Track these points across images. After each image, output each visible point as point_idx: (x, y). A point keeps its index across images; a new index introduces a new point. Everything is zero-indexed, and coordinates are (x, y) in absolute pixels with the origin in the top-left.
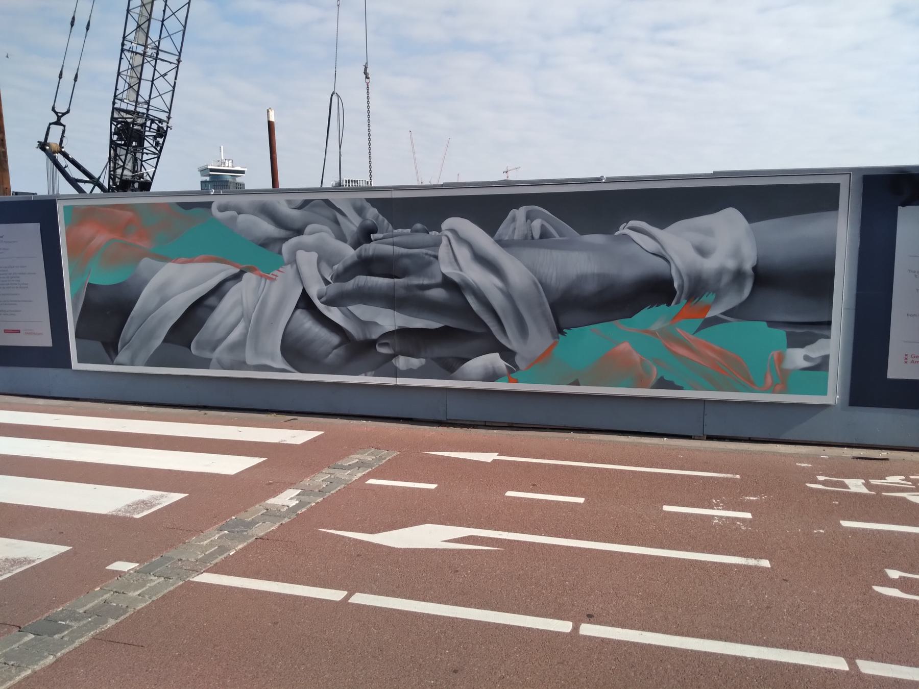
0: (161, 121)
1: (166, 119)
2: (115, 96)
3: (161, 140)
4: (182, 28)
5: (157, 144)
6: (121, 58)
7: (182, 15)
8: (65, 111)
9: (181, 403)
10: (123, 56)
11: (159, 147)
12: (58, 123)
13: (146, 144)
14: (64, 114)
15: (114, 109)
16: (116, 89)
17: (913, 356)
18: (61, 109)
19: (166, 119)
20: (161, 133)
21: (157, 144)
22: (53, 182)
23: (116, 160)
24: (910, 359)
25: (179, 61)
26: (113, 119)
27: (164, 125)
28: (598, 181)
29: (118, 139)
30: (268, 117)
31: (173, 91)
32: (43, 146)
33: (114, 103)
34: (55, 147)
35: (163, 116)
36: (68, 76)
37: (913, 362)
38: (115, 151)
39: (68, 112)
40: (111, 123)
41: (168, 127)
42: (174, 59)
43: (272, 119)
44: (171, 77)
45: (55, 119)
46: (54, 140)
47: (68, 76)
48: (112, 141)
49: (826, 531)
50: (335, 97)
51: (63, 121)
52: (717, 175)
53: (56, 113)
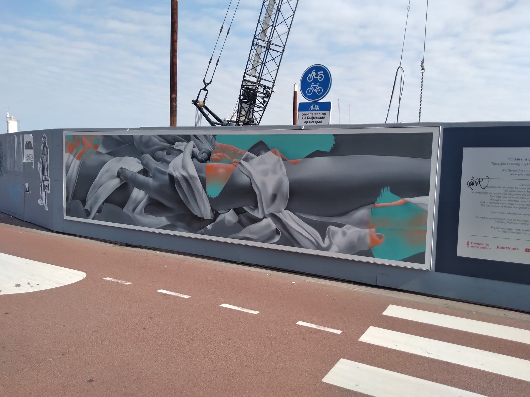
0: (269, 88)
1: (271, 87)
2: (245, 73)
3: (267, 100)
4: (288, 30)
5: (264, 101)
6: (251, 49)
7: (289, 21)
8: (209, 82)
9: (340, 277)
10: (253, 48)
11: (265, 104)
12: (205, 89)
13: (257, 102)
14: (208, 84)
15: (244, 80)
16: (246, 68)
17: (472, 243)
18: (207, 81)
19: (271, 87)
20: (268, 95)
21: (264, 101)
22: (198, 120)
23: (241, 111)
24: (470, 245)
25: (283, 51)
26: (242, 86)
27: (270, 91)
28: (124, 130)
29: (243, 99)
30: (294, 89)
31: (278, 69)
32: (195, 103)
33: (244, 77)
34: (202, 104)
35: (270, 85)
36: (214, 61)
37: (472, 246)
38: (241, 105)
39: (210, 83)
40: (241, 89)
41: (272, 91)
42: (280, 49)
43: (296, 90)
44: (277, 60)
45: (203, 87)
46: (201, 99)
47: (214, 61)
48: (240, 100)
49: (297, 283)
50: (400, 70)
51: (207, 88)
52: (131, 129)
53: (205, 83)
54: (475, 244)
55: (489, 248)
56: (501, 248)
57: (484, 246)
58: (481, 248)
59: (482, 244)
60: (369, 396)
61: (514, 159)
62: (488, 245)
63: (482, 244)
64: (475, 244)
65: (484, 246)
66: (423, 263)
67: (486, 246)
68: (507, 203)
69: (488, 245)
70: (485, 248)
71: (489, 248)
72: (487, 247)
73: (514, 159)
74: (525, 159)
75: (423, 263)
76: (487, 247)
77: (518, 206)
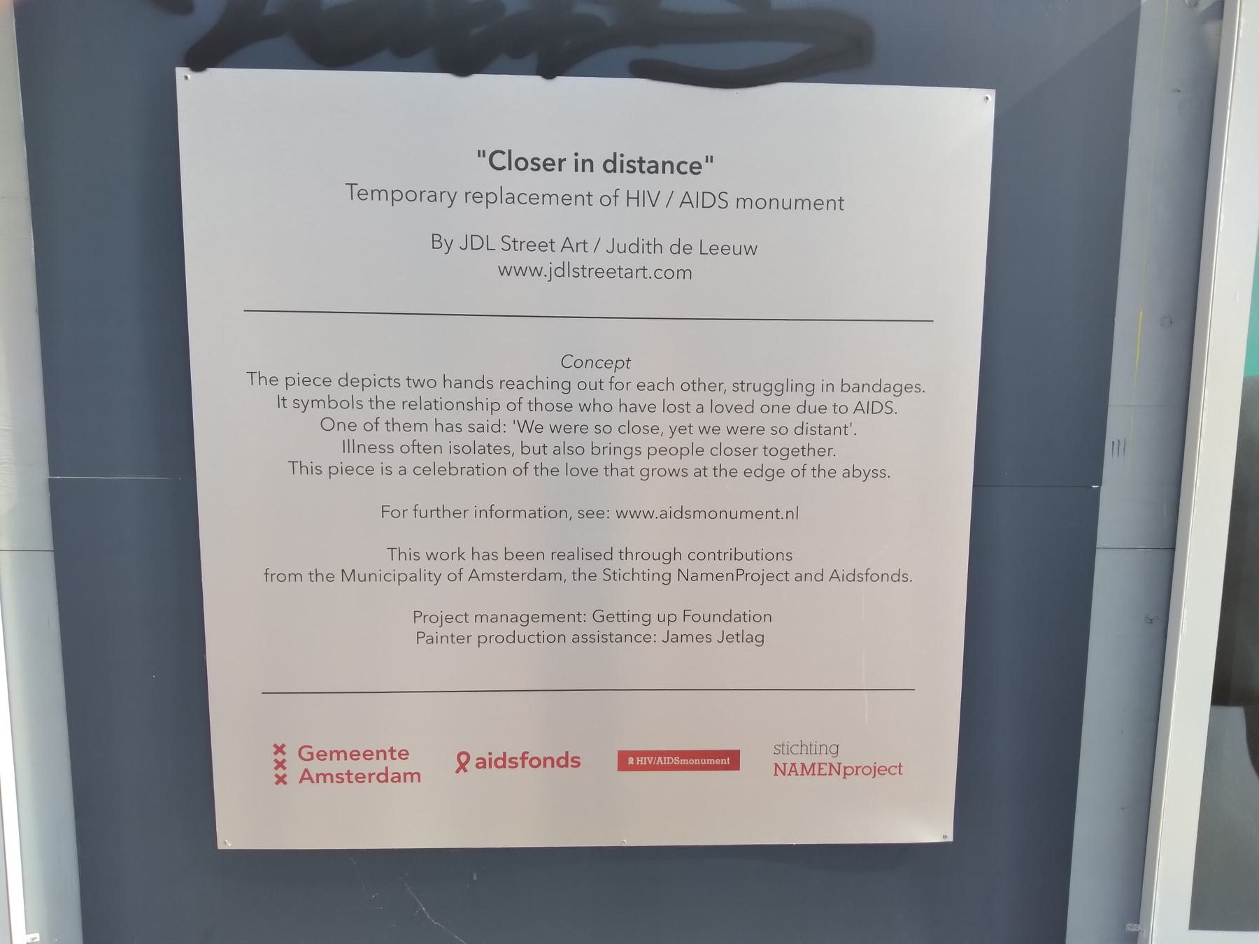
24: (295, 768)
37: (306, 776)
54: (321, 755)
55: (414, 776)
56: (482, 764)
57: (377, 766)
58: (360, 778)
59: (368, 755)
60: (214, 65)
61: (518, 164)
62: (404, 754)
63: (368, 755)
64: (321, 755)
65: (377, 766)
66: (1202, 917)
67: (387, 767)
68: (511, 437)
69: (404, 754)
70: (384, 777)
71: (414, 776)
72: (398, 766)
73: (518, 164)
74: (584, 164)
75: (1202, 917)
76: (398, 766)
77: (676, 397)
